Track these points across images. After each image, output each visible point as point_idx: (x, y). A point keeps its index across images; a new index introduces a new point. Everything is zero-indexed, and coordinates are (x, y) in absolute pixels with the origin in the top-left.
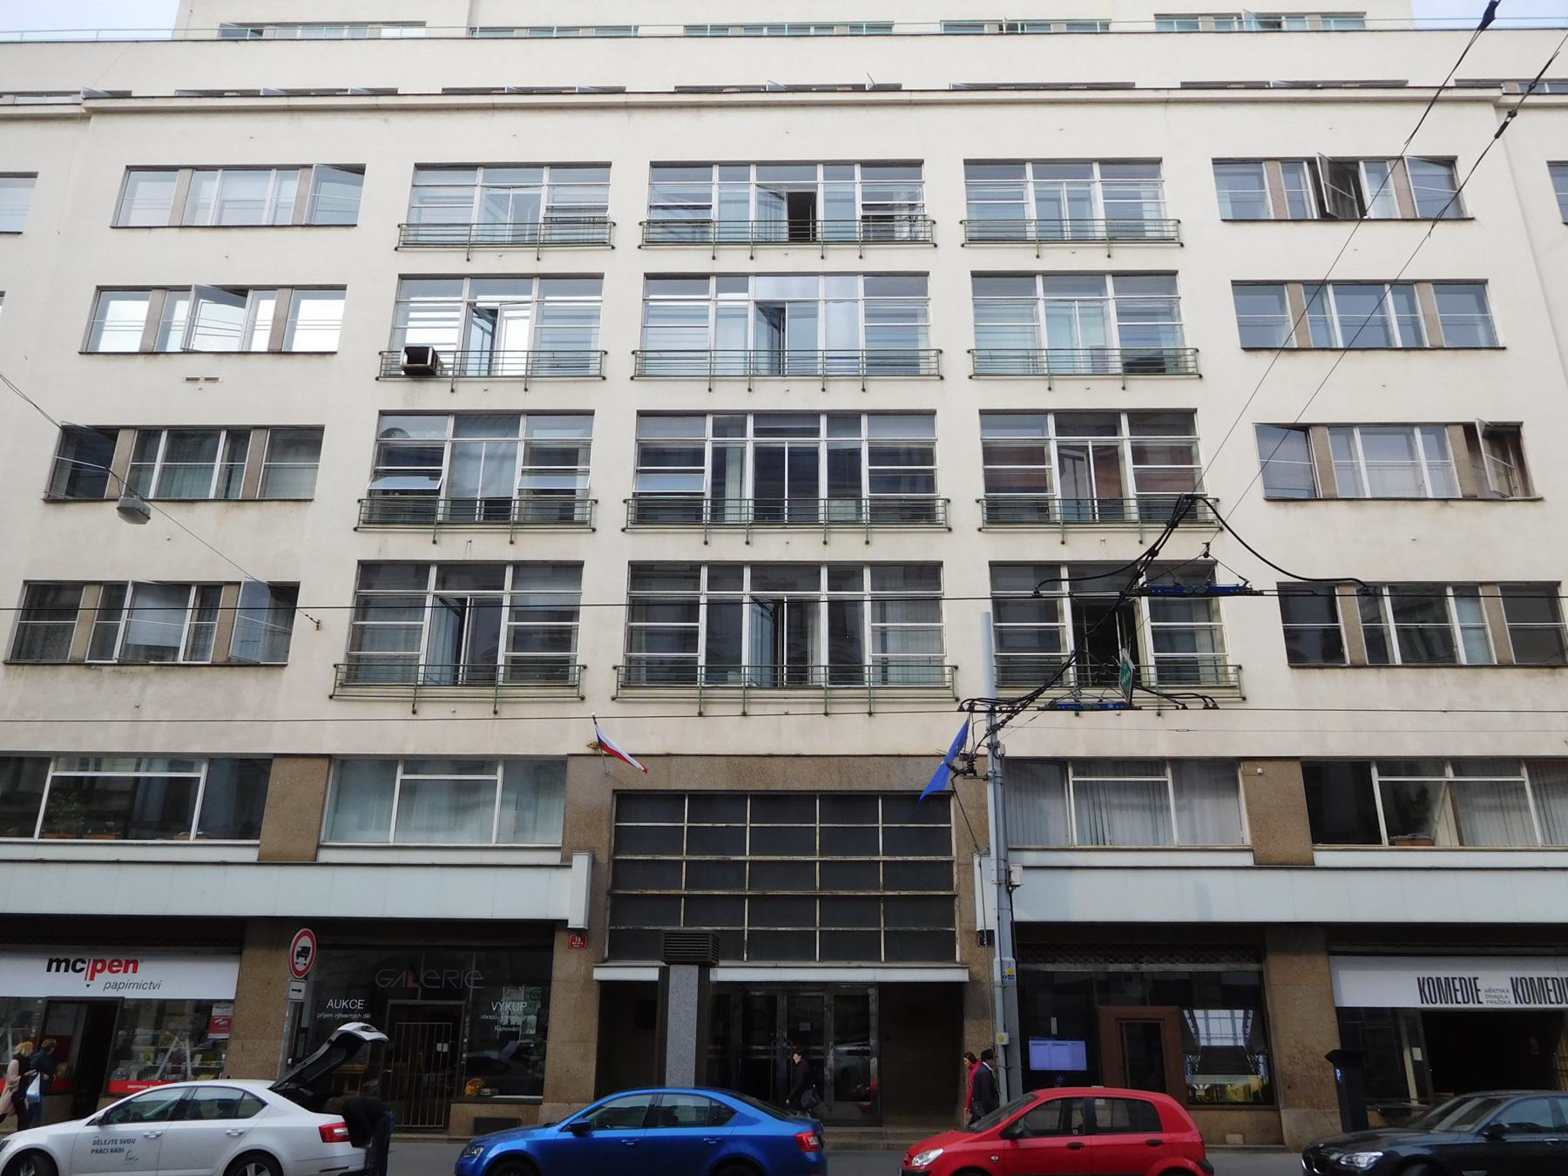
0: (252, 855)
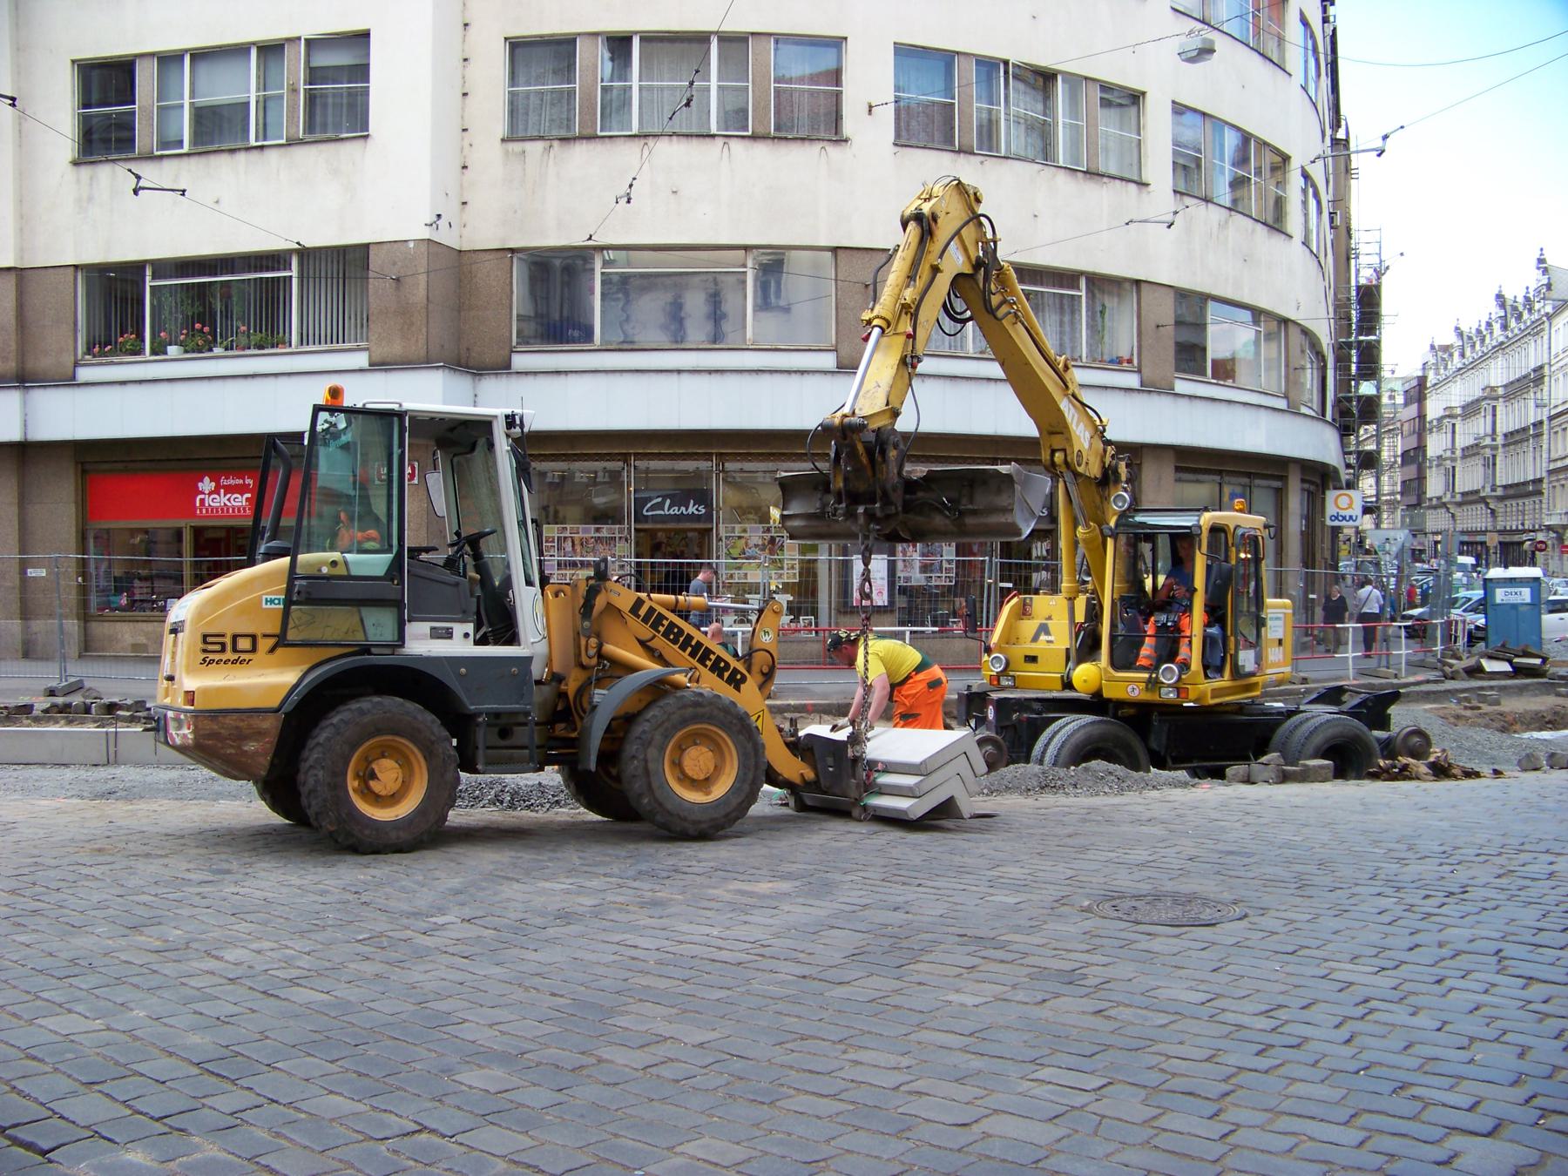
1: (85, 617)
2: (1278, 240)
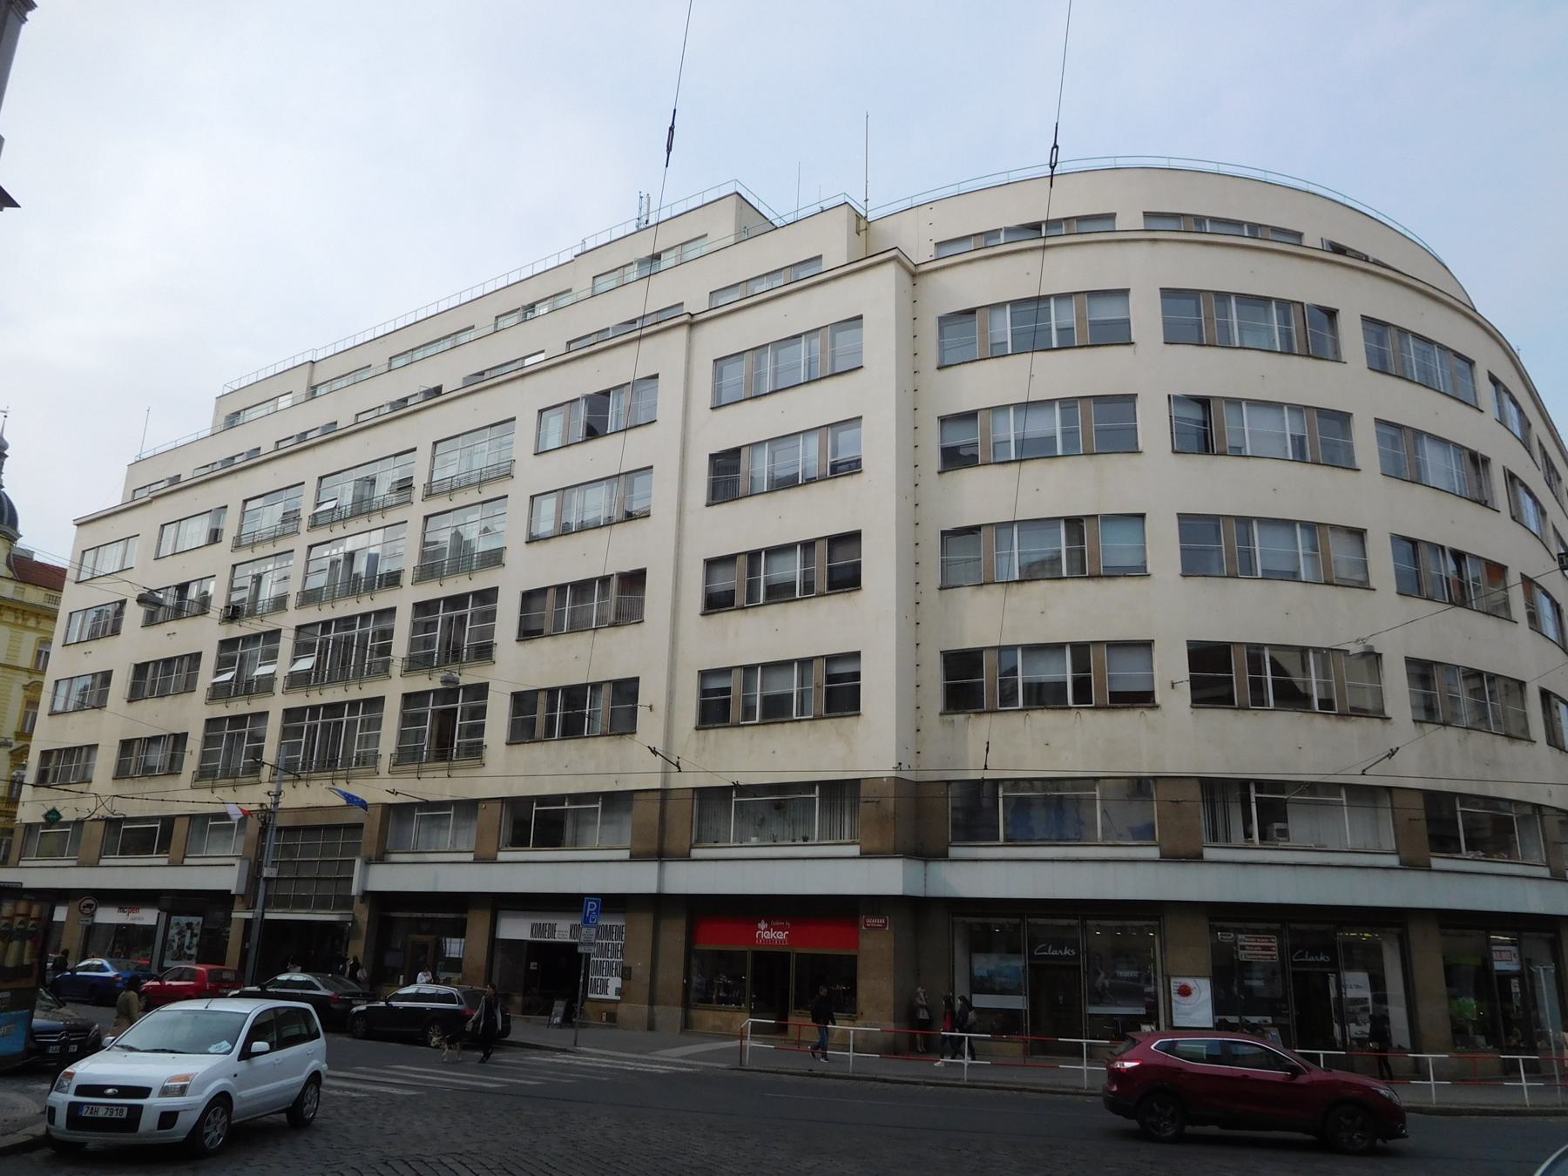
0: (165, 861)
1: (687, 1005)
2: (1519, 748)
